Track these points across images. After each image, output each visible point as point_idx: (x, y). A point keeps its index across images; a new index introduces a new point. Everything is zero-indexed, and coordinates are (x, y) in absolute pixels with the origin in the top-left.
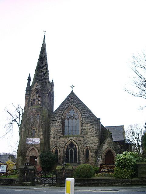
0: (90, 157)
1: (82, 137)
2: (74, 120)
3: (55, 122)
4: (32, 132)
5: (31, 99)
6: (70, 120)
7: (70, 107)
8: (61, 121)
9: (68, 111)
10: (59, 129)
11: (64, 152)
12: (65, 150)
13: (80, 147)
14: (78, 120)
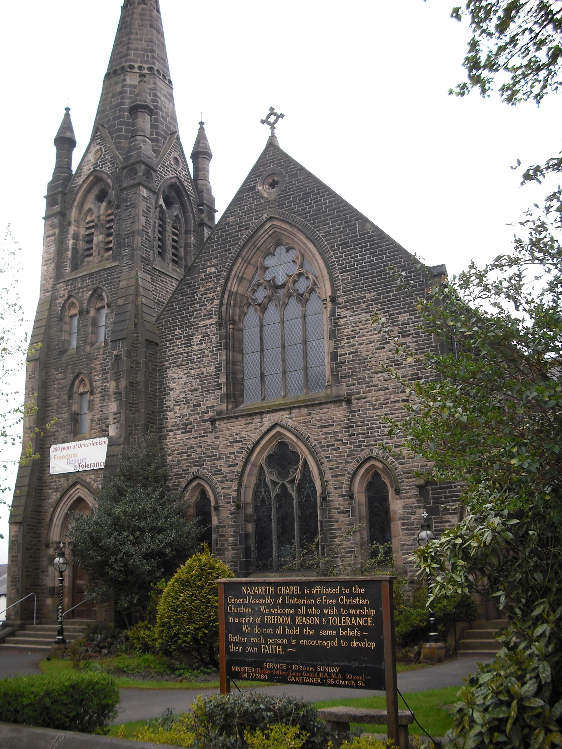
0: (397, 527)
1: (337, 401)
2: (294, 308)
3: (189, 338)
4: (75, 408)
5: (70, 236)
6: (272, 313)
7: (263, 236)
8: (220, 325)
9: (258, 259)
10: (212, 369)
11: (238, 507)
12: (248, 496)
13: (327, 465)
14: (314, 304)
